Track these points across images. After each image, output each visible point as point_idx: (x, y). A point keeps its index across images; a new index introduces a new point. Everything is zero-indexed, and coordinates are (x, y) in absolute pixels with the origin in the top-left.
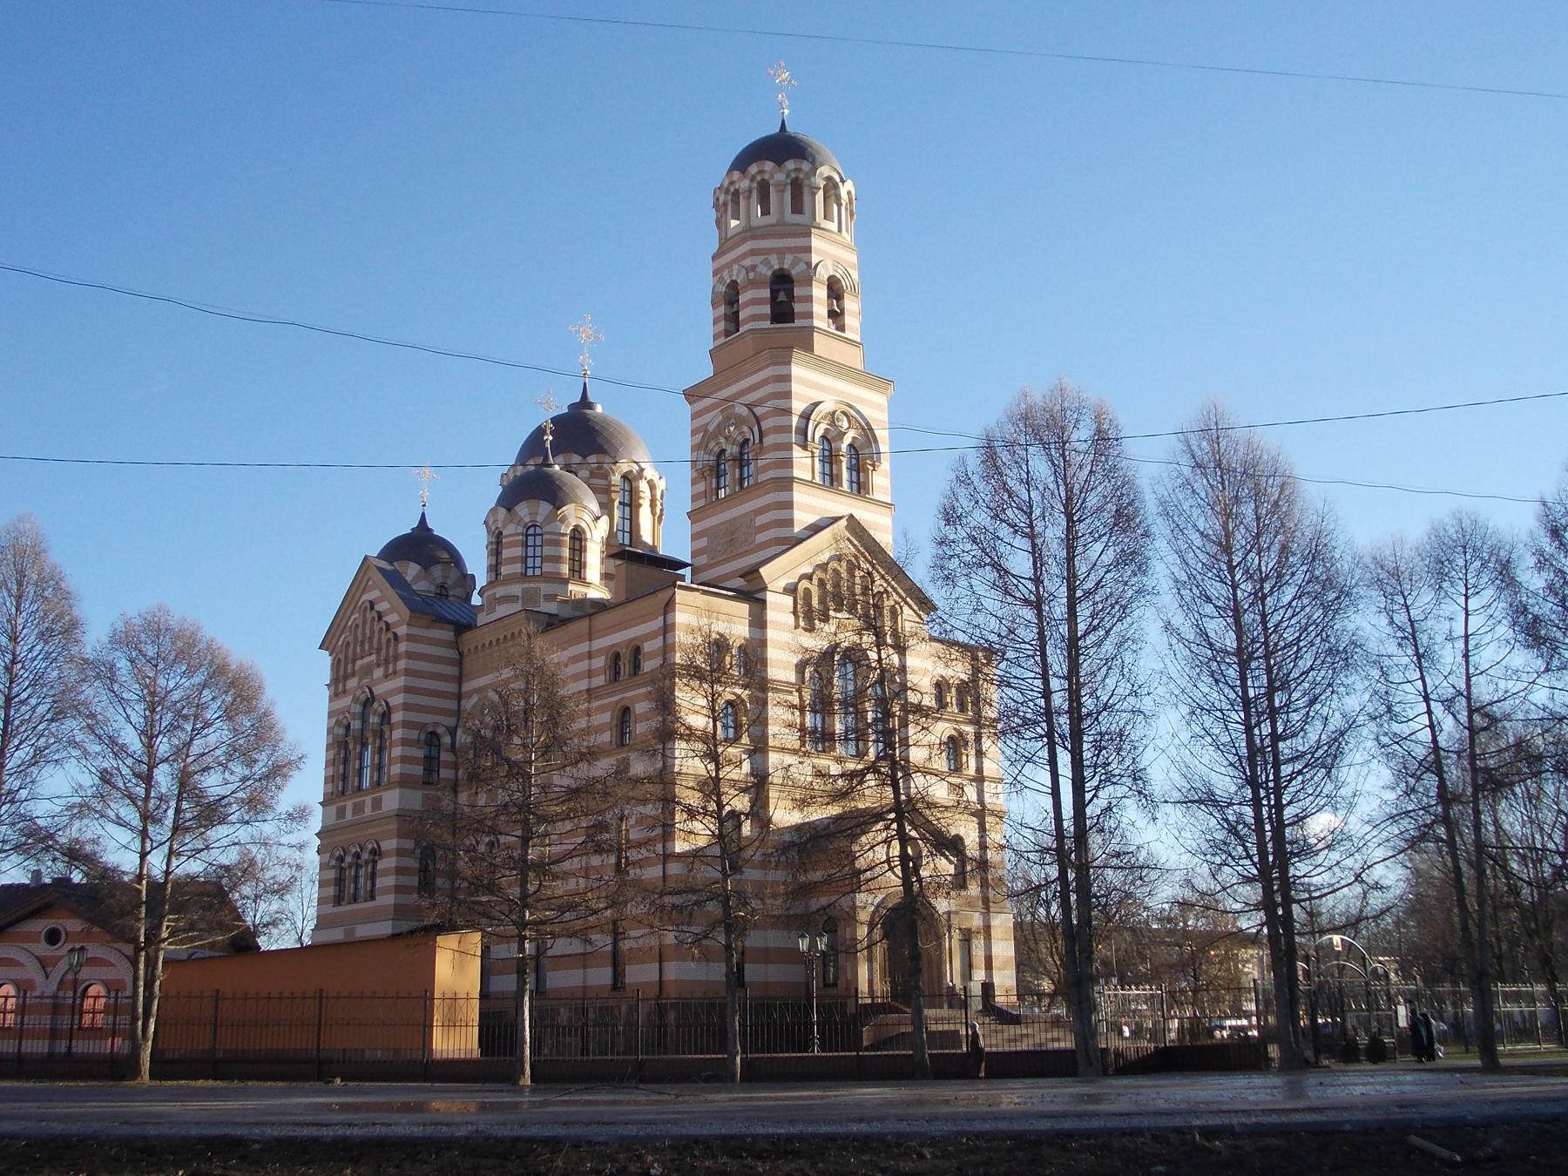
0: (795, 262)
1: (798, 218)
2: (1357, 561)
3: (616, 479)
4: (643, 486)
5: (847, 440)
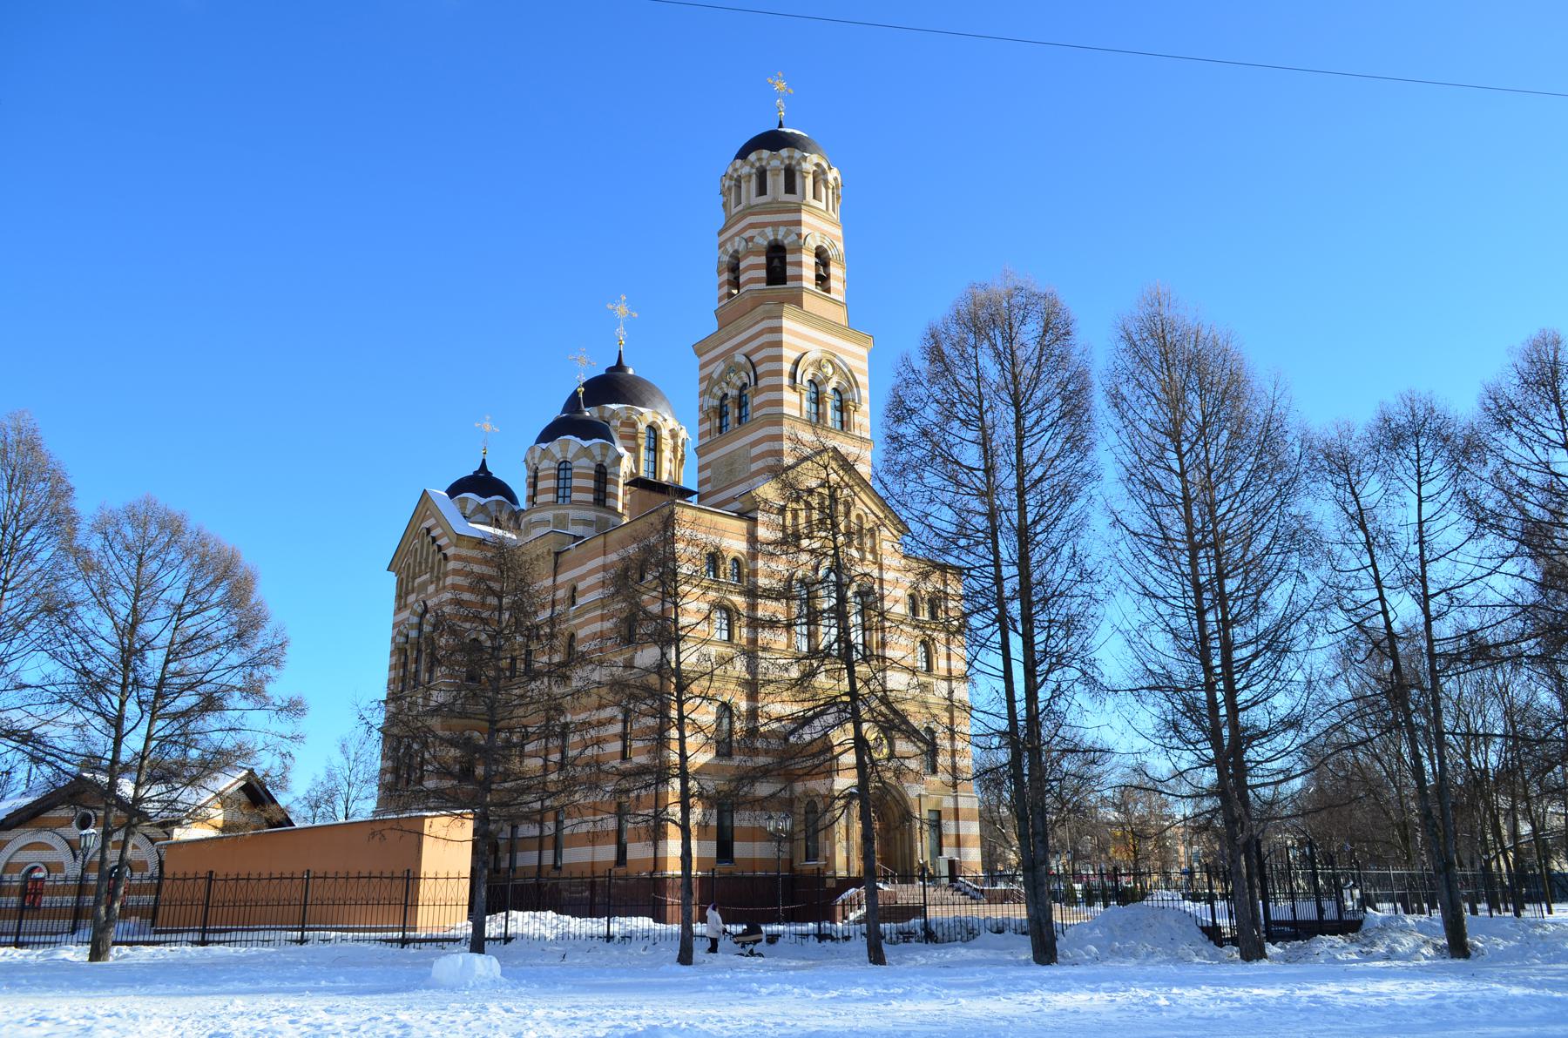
0: (787, 234)
1: (790, 198)
2: (1306, 443)
3: (642, 427)
4: (665, 433)
5: (832, 384)
